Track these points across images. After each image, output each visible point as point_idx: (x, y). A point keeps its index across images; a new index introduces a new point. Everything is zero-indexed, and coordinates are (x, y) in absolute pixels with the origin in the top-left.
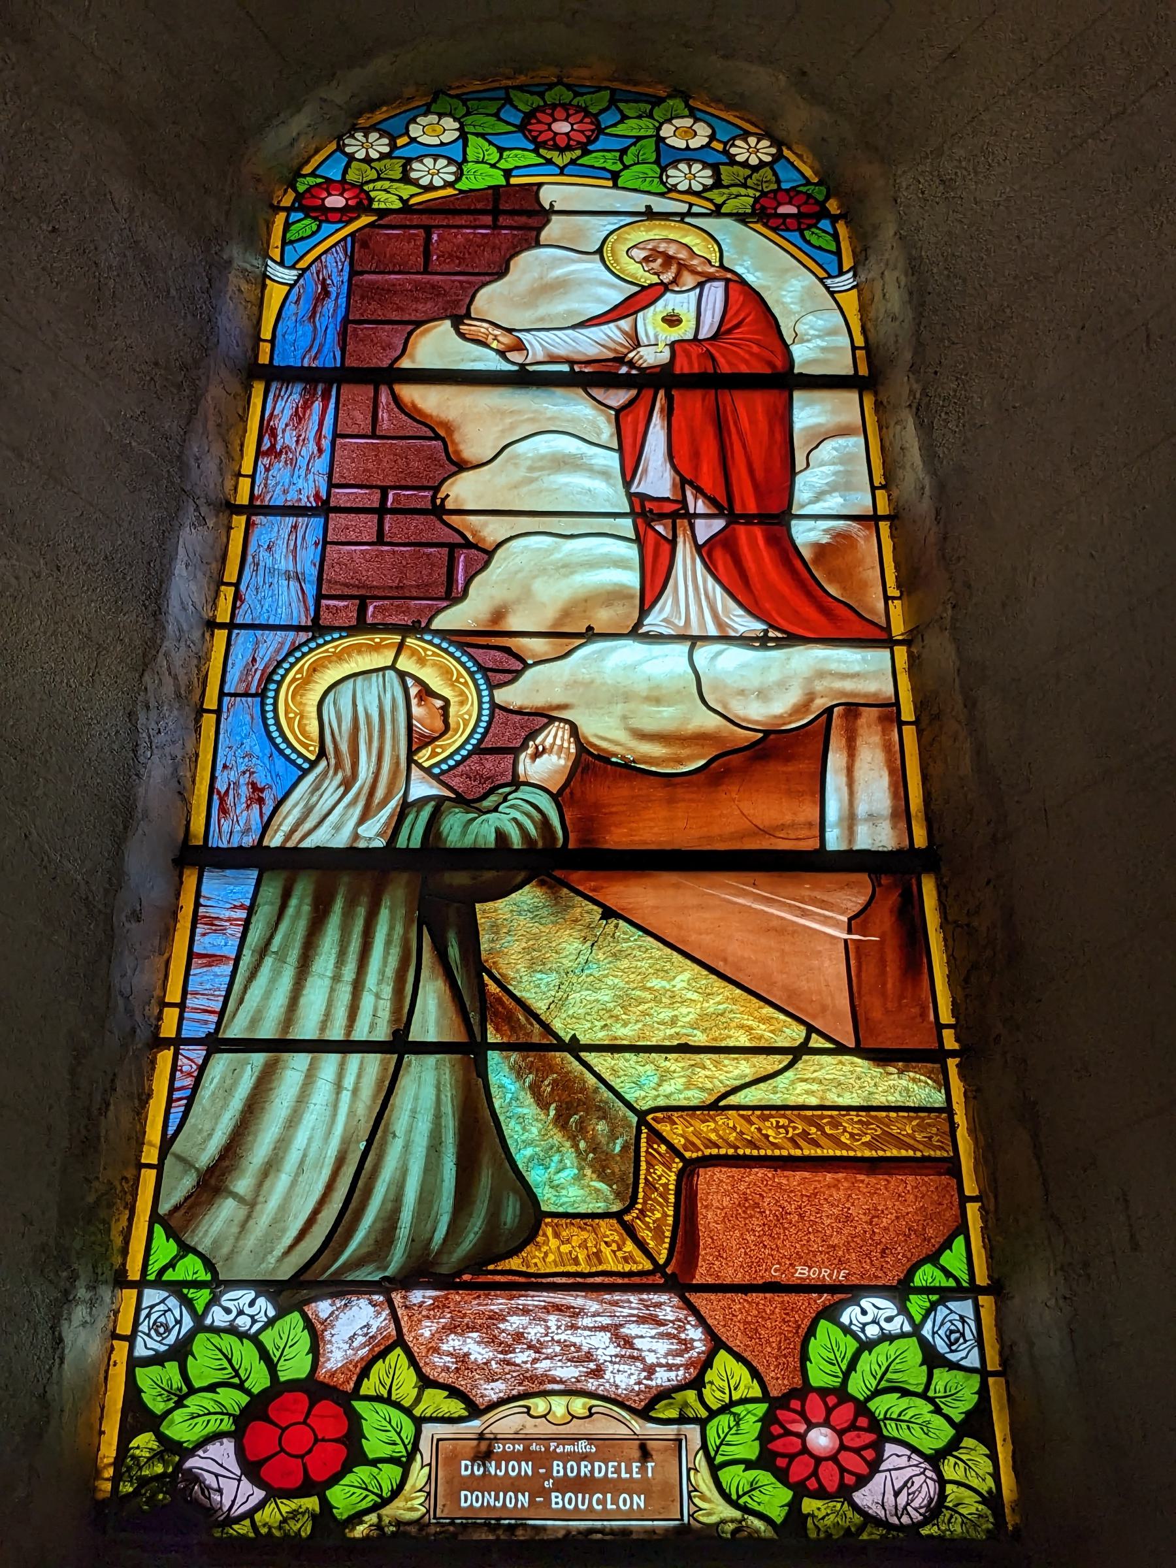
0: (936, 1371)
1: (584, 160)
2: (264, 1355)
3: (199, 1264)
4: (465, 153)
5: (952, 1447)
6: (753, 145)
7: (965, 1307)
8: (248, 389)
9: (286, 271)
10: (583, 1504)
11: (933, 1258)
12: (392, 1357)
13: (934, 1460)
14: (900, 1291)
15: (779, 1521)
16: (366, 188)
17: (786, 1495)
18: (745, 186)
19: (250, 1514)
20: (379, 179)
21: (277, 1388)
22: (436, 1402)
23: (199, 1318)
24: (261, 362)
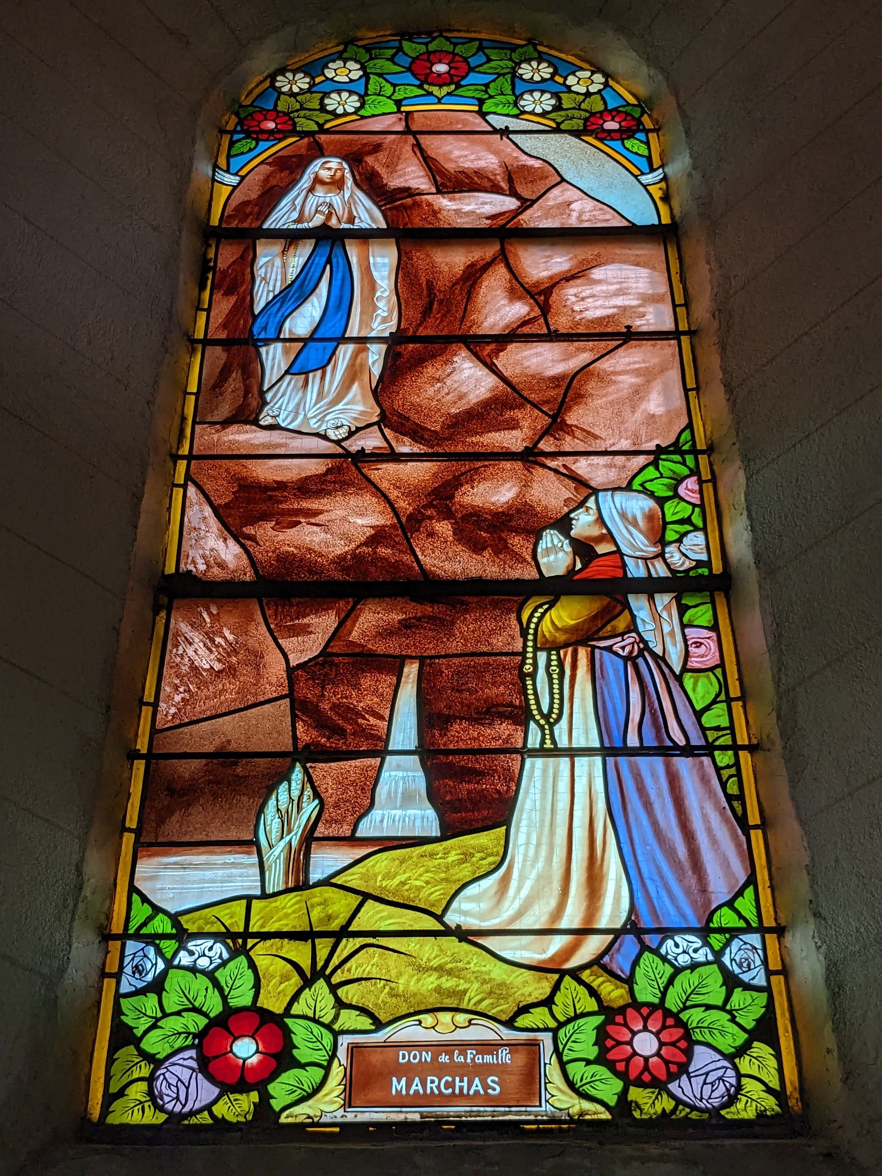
1: (459, 92)
2: (216, 984)
4: (366, 89)
5: (742, 1050)
9: (232, 177)
16: (292, 115)
17: (618, 1085)
19: (208, 1108)
20: (302, 108)
21: (229, 1012)
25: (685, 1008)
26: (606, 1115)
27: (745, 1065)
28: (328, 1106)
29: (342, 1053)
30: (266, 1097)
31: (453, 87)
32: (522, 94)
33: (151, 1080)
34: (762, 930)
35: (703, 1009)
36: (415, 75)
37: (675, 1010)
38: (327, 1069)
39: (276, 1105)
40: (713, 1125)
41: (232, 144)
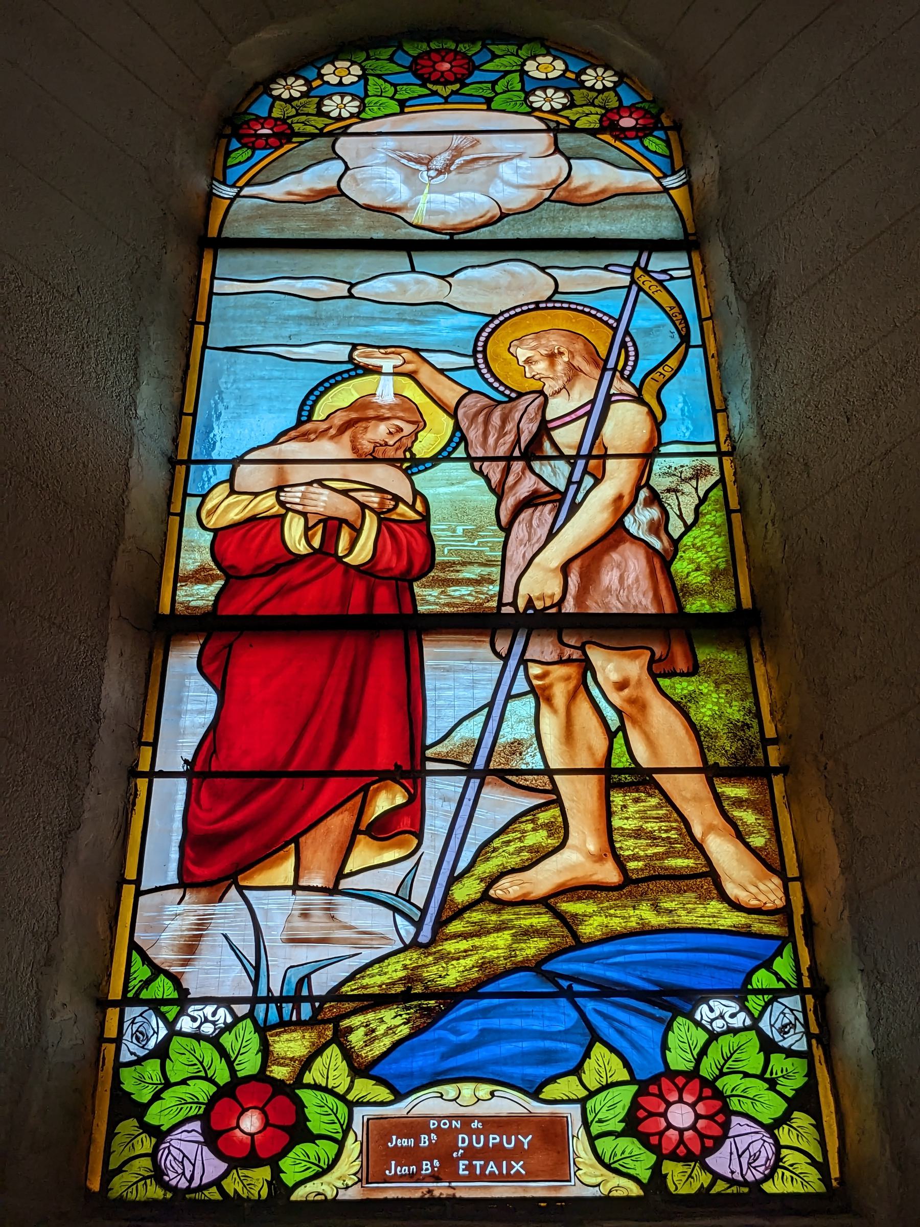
0: (772, 1056)
1: (465, 90)
2: (223, 1053)
3: (169, 984)
4: (366, 90)
5: (784, 1119)
6: (600, 74)
7: (793, 1001)
8: (200, 259)
9: (229, 189)
10: (478, 1142)
11: (767, 965)
12: (328, 1051)
13: (771, 1128)
14: (740, 994)
15: (645, 1181)
16: (289, 121)
17: (652, 1158)
18: (593, 104)
19: (217, 1183)
20: (298, 114)
21: (236, 1081)
22: (365, 1088)
23: (170, 1025)
24: (209, 235)
25: (722, 1074)
26: (635, 1190)
27: (785, 1135)
28: (342, 1181)
29: (357, 1126)
30: (277, 1171)
31: (458, 86)
32: (535, 90)
33: (153, 1155)
34: (800, 990)
35: (741, 1075)
36: (416, 75)
37: (710, 1078)
38: (341, 1144)
39: (289, 1178)
40: (751, 1198)
41: (228, 154)
